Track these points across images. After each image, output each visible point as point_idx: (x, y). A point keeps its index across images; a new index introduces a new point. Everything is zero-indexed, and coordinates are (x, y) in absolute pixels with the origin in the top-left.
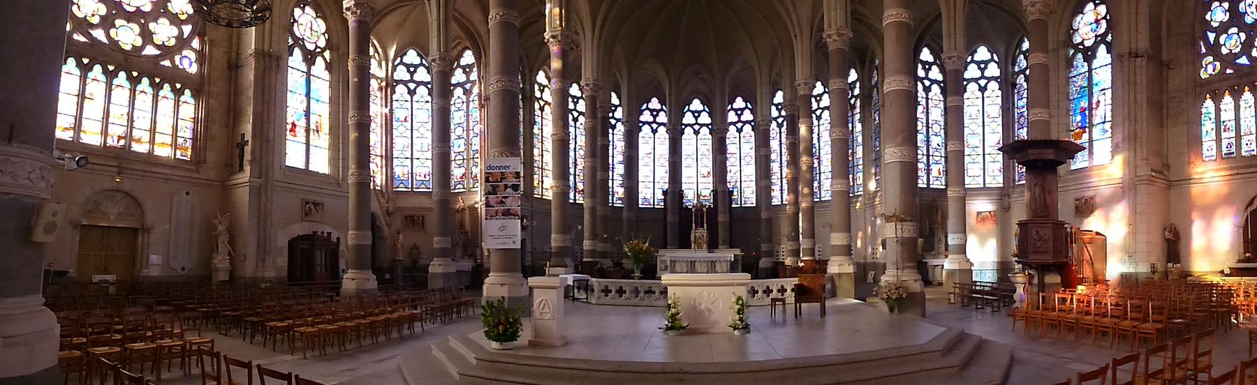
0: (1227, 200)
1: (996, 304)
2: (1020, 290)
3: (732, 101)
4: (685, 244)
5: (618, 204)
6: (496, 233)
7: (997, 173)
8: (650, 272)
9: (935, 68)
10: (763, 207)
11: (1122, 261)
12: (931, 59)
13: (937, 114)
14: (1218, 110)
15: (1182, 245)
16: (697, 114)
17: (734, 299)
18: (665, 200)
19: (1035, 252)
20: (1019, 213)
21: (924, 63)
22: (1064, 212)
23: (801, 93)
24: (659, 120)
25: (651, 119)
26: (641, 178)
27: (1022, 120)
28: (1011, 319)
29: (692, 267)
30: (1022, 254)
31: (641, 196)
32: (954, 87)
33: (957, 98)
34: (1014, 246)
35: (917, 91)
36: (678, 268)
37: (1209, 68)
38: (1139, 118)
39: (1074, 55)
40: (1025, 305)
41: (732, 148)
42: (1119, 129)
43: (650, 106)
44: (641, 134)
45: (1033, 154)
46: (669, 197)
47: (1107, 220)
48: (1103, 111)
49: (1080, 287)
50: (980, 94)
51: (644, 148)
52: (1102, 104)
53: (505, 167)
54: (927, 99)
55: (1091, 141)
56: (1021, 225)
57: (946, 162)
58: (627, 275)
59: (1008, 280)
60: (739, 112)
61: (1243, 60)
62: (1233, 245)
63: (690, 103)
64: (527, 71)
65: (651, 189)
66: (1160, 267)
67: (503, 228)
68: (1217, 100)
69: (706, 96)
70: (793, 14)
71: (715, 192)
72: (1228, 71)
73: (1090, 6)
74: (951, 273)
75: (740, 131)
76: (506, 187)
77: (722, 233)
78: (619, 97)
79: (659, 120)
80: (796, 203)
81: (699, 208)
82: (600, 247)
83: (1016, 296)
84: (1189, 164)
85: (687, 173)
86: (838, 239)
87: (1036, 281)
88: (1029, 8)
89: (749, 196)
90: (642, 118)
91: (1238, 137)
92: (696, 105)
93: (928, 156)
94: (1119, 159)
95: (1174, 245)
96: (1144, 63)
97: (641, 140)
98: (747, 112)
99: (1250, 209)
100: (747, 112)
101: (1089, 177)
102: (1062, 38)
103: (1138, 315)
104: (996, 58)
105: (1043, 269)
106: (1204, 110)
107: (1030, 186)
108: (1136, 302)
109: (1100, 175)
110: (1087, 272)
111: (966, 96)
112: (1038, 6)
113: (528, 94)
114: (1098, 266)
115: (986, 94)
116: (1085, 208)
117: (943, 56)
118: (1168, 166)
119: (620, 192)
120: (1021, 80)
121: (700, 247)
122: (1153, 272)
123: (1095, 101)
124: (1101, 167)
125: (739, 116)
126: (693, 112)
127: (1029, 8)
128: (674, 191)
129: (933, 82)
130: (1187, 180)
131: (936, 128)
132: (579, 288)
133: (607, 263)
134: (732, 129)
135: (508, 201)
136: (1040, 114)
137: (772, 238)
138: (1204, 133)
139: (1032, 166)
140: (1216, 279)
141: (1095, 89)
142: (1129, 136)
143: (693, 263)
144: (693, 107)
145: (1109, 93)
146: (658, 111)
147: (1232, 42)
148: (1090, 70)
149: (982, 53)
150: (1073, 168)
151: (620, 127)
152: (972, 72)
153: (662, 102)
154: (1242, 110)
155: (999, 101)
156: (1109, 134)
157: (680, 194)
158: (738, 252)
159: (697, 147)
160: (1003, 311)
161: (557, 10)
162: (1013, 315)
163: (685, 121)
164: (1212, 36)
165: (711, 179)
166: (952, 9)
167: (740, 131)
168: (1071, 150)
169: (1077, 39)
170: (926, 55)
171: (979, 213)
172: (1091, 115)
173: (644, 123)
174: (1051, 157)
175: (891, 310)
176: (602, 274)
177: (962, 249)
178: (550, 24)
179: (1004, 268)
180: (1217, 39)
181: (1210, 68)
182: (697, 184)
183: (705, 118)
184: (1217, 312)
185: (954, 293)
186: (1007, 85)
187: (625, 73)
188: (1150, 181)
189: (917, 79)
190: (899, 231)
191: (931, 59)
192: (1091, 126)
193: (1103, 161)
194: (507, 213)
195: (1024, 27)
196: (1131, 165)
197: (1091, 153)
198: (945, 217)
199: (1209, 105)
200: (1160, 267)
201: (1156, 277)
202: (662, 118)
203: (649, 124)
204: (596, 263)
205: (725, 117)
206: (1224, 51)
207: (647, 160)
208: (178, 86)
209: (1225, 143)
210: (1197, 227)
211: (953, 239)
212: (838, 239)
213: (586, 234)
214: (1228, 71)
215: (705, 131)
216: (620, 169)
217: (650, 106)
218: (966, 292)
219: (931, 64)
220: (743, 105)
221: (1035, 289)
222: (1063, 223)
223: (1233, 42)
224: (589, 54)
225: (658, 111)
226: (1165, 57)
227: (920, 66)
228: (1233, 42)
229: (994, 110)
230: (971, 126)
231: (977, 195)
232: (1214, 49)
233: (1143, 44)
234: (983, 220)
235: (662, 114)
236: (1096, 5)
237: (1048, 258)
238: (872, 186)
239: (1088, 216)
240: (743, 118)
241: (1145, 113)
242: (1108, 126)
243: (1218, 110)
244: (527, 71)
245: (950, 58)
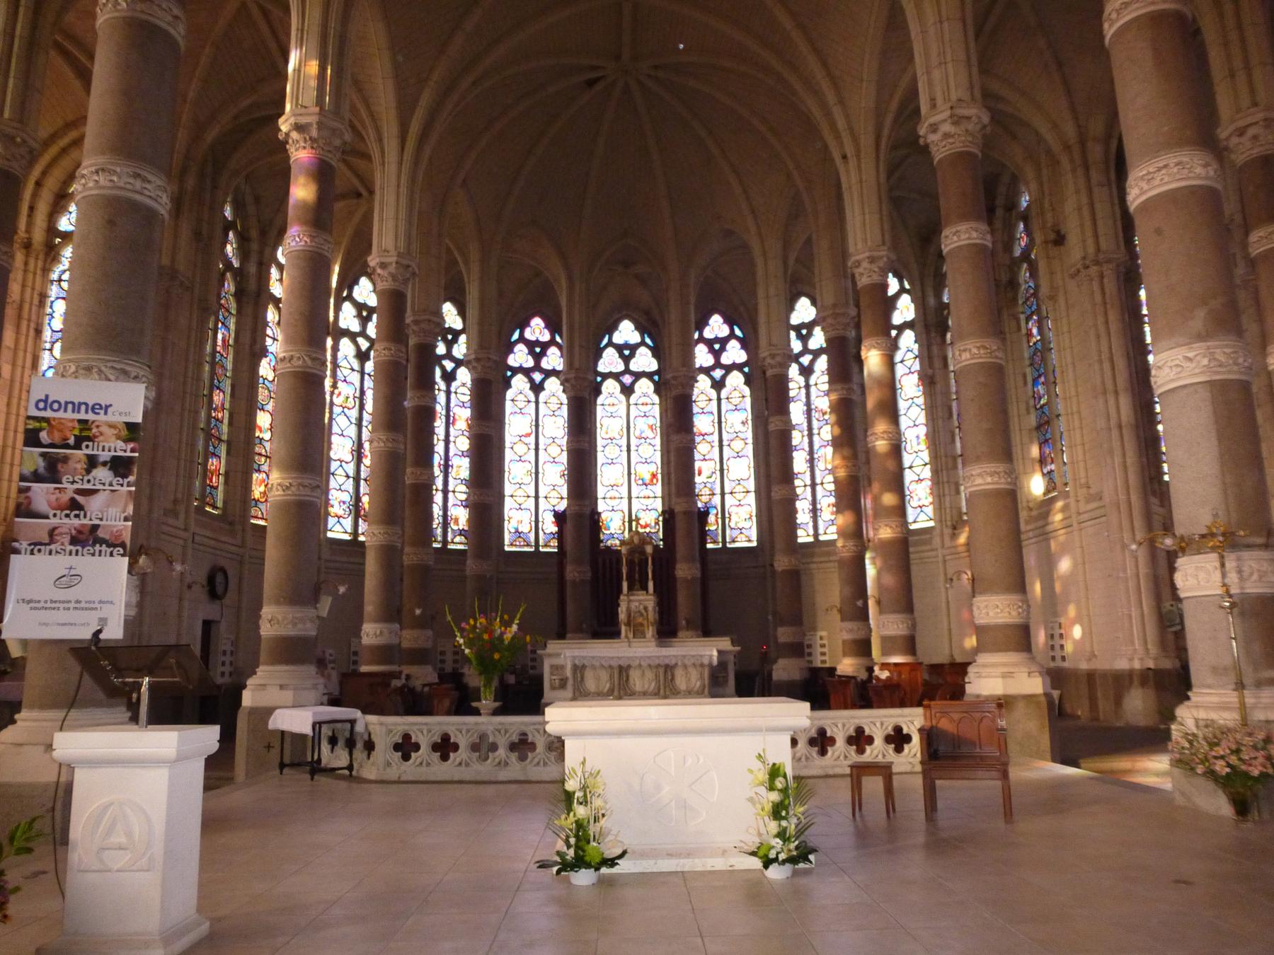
3: (702, 323)
4: (605, 627)
5: (458, 544)
6: (48, 592)
8: (525, 696)
10: (779, 544)
16: (627, 352)
17: (763, 776)
18: (560, 535)
23: (863, 281)
24: (546, 364)
25: (530, 363)
26: (508, 489)
29: (620, 686)
31: (509, 527)
36: (590, 684)
41: (702, 423)
43: (528, 334)
44: (510, 394)
46: (569, 526)
50: (713, 394)
51: (516, 425)
53: (94, 408)
58: (464, 704)
60: (717, 347)
63: (612, 328)
64: (254, 234)
65: (531, 508)
67: (68, 580)
69: (647, 313)
70: (837, 112)
71: (669, 517)
75: (718, 385)
76: (92, 462)
77: (685, 603)
78: (462, 313)
79: (546, 364)
80: (856, 534)
81: (638, 543)
82: (410, 638)
85: (608, 476)
86: (995, 609)
89: (740, 524)
90: (513, 361)
92: (626, 332)
97: (509, 407)
98: (733, 346)
100: (733, 346)
113: (252, 285)
119: (461, 516)
121: (638, 632)
125: (717, 354)
126: (619, 348)
128: (581, 515)
132: (333, 741)
133: (423, 676)
134: (703, 383)
135: (94, 505)
137: (798, 612)
143: (623, 671)
144: (618, 338)
146: (545, 346)
151: (464, 376)
153: (553, 327)
157: (592, 522)
158: (725, 643)
161: (313, 67)
163: (602, 367)
165: (658, 489)
167: (718, 385)
173: (516, 371)
175: (1242, 808)
176: (415, 704)
178: (296, 98)
182: (630, 502)
183: (645, 361)
187: (474, 255)
190: (1233, 578)
194: (87, 538)
202: (554, 359)
203: (527, 372)
204: (397, 675)
205: (689, 356)
207: (521, 449)
208: (599, 379)
212: (995, 609)
213: (369, 608)
215: (645, 386)
216: (462, 468)
217: (528, 334)
220: (724, 331)
224: (390, 198)
225: (545, 346)
235: (553, 351)
238: (1036, 485)
240: (726, 359)
244: (254, 234)
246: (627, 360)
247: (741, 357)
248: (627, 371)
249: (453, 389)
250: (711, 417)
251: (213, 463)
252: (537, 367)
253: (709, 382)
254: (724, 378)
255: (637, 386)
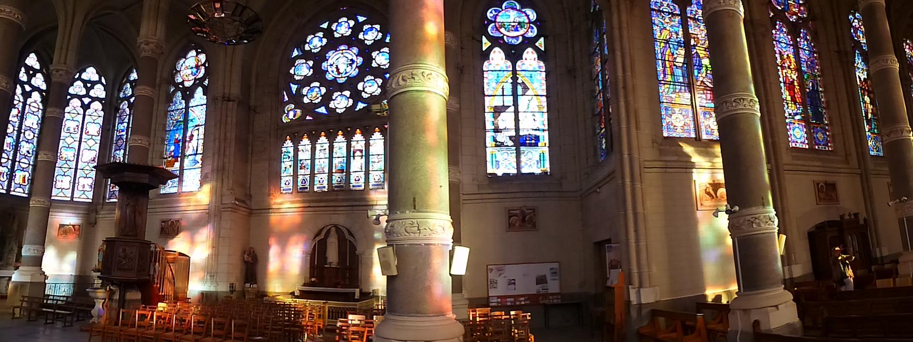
0: (299, 229)
1: (69, 319)
2: (99, 305)
7: (87, 188)
9: (39, 75)
11: (203, 280)
12: (37, 66)
13: (32, 121)
14: (296, 151)
15: (259, 267)
19: (119, 269)
20: (106, 230)
21: (28, 68)
22: (151, 233)
25: (84, 92)
27: (120, 142)
28: (87, 335)
30: (106, 270)
32: (55, 99)
33: (58, 110)
34: (96, 260)
35: (15, 94)
37: (291, 114)
38: (227, 153)
39: (175, 92)
40: (102, 321)
42: (209, 162)
45: (129, 176)
47: (192, 242)
48: (196, 143)
49: (160, 304)
50: (81, 111)
52: (195, 138)
54: (25, 104)
55: (182, 169)
56: (108, 242)
57: (34, 170)
59: (87, 294)
61: (322, 110)
62: (302, 268)
66: (238, 287)
68: (296, 142)
72: (308, 118)
73: (193, 53)
74: (20, 286)
83: (94, 312)
84: (269, 195)
87: (116, 297)
88: (143, 46)
91: (313, 175)
93: (14, 161)
94: (207, 188)
95: (252, 267)
96: (235, 106)
99: (317, 239)
101: (178, 201)
102: (165, 75)
103: (221, 332)
104: (103, 80)
105: (125, 286)
106: (284, 150)
107: (122, 205)
108: (218, 320)
109: (188, 201)
110: (168, 289)
111: (67, 109)
112: (151, 45)
114: (179, 284)
115: (88, 112)
116: (171, 229)
117: (52, 68)
118: (250, 197)
120: (125, 106)
122: (232, 292)
123: (189, 134)
124: (191, 193)
127: (143, 46)
129: (35, 89)
130: (267, 209)
131: (29, 135)
136: (140, 141)
138: (283, 169)
139: (125, 188)
140: (288, 300)
141: (190, 124)
142: (217, 167)
145: (202, 129)
147: (313, 94)
148: (187, 107)
149: (91, 74)
150: (162, 192)
152: (77, 88)
154: (317, 152)
155: (100, 121)
156: (199, 165)
159: (322, 163)
160: (77, 326)
162: (90, 330)
164: (294, 88)
166: (69, 25)
168: (167, 176)
169: (179, 79)
170: (32, 60)
171: (62, 226)
172: (184, 147)
173: (74, 96)
174: (146, 181)
177: (37, 261)
179: (81, 282)
180: (298, 90)
181: (291, 115)
184: (289, 331)
185: (21, 308)
186: (111, 107)
188: (234, 209)
189: (18, 81)
191: (37, 66)
192: (183, 156)
193: (193, 188)
195: (135, 61)
196: (217, 194)
197: (181, 181)
198: (22, 227)
199: (289, 143)
200: (238, 287)
201: (234, 296)
206: (306, 100)
209: (300, 178)
210: (274, 251)
211: (27, 251)
214: (308, 118)
218: (34, 306)
219: (36, 71)
220: (95, 77)
221: (115, 305)
222: (148, 244)
223: (314, 94)
226: (252, 103)
227: (23, 69)
228: (314, 94)
229: (94, 129)
230: (68, 140)
231: (63, 208)
232: (297, 99)
233: (235, 90)
234: (65, 232)
236: (198, 53)
237: (132, 276)
239: (173, 237)
241: (233, 149)
242: (199, 158)
243: (296, 151)
245: (57, 71)
246: (88, 90)
247: (102, 95)
248: (87, 95)
249: (28, 103)
250: (77, 123)
251: (864, 76)
252: (29, 83)
253: (79, 103)
254: (31, 92)
255: (92, 105)
